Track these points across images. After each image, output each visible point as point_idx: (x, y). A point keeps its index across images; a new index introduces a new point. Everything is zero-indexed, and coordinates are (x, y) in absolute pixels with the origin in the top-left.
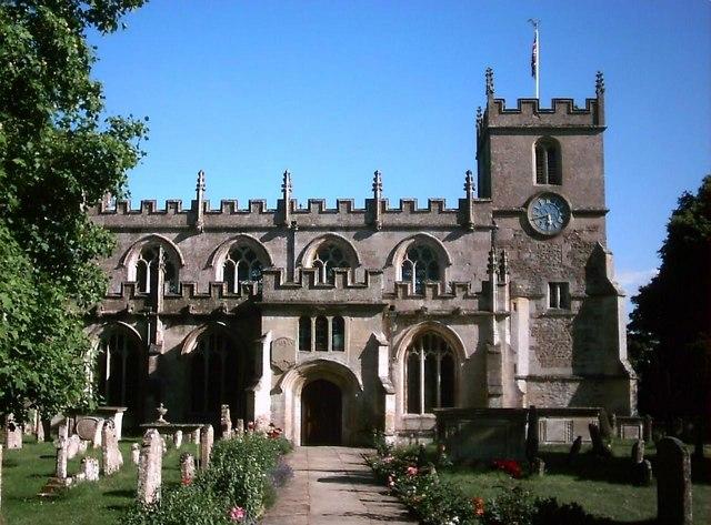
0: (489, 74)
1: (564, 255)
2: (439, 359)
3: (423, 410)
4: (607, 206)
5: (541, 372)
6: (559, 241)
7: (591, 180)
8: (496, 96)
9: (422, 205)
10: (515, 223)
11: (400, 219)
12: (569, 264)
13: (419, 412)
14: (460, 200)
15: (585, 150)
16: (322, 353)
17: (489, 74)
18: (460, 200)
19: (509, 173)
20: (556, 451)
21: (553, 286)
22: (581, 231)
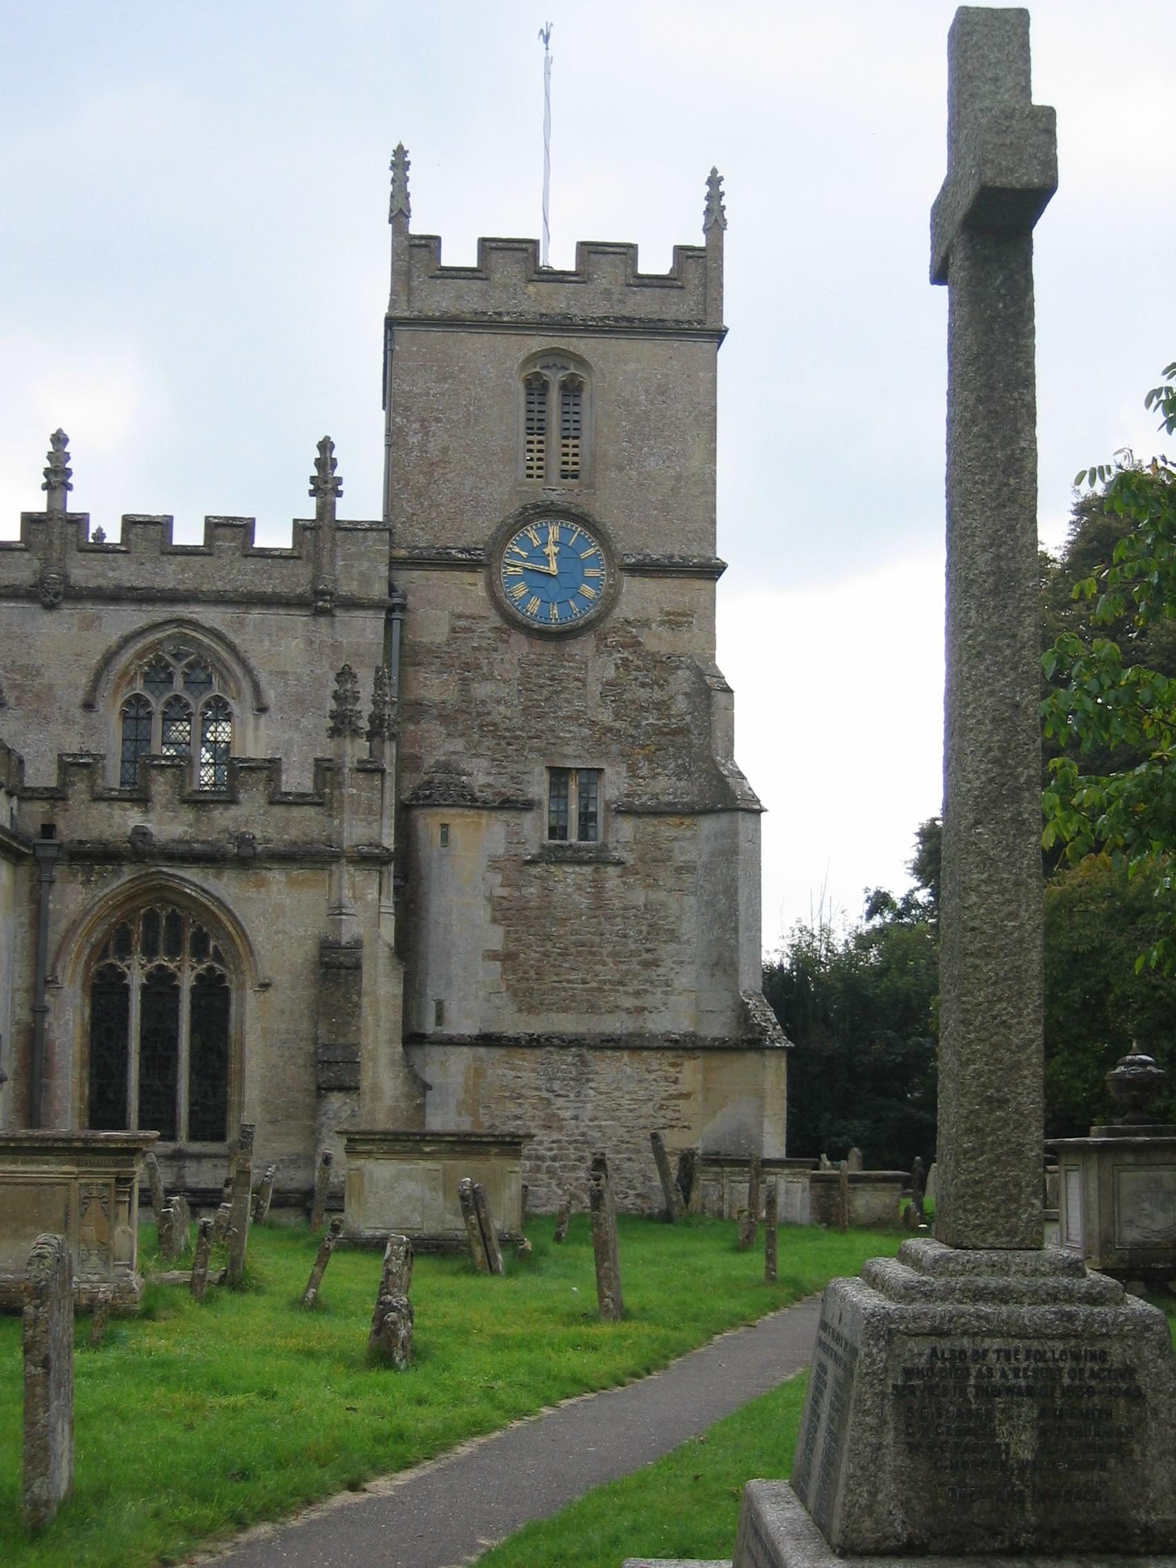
0: (400, 162)
1: (595, 688)
2: (187, 981)
3: (133, 1117)
4: (722, 553)
5: (515, 1024)
6: (584, 647)
7: (678, 478)
8: (417, 227)
9: (189, 533)
10: (474, 587)
11: (127, 574)
12: (605, 716)
13: (171, 1136)
14: (632, 248)
15: (662, 391)
16: (598, 818)
17: (400, 162)
18: (632, 248)
19: (445, 450)
20: (87, 1092)
21: (559, 775)
22: (645, 624)
